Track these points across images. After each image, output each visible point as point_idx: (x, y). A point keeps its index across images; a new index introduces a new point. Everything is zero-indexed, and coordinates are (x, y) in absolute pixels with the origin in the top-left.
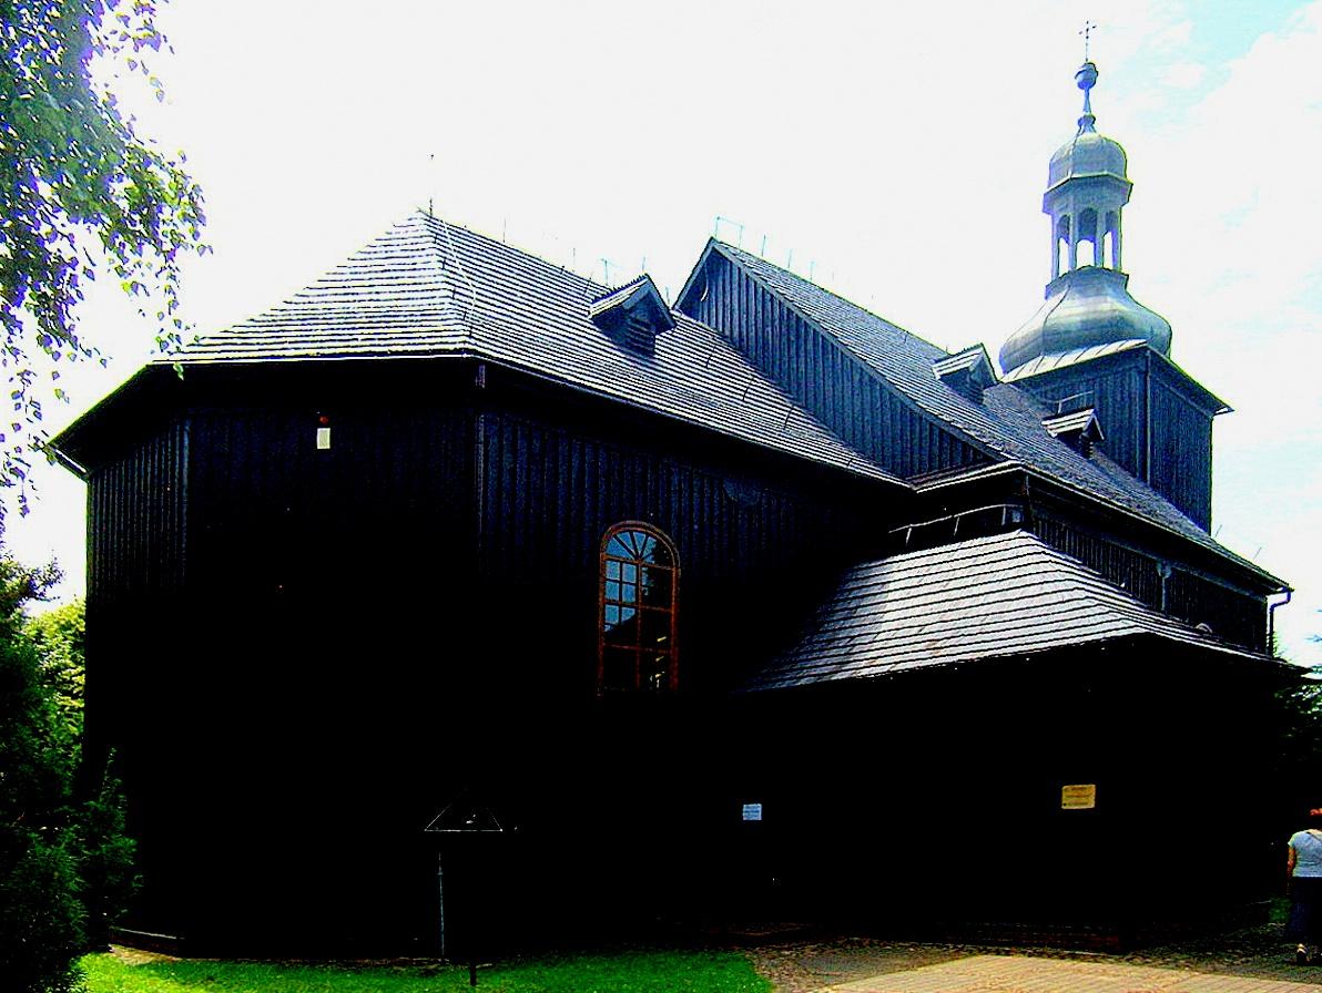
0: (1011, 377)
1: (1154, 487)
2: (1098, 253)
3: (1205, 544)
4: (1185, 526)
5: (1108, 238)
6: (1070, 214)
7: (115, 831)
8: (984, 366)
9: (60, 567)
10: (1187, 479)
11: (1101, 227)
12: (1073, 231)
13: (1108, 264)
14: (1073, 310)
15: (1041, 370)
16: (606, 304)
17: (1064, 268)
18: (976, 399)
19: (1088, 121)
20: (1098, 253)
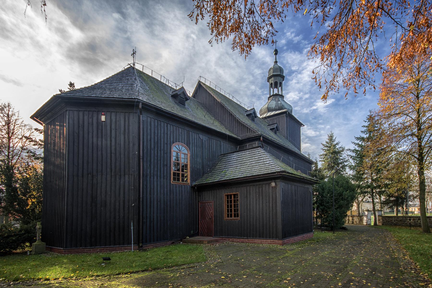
0: (261, 117)
1: (295, 169)
2: (278, 91)
3: (299, 153)
4: (296, 150)
5: (280, 88)
6: (273, 82)
7: (21, 180)
8: (255, 113)
9: (72, 83)
10: (295, 137)
11: (278, 85)
12: (273, 86)
13: (280, 93)
14: (273, 104)
15: (267, 115)
16: (174, 93)
17: (272, 94)
18: (253, 120)
19: (276, 62)
20: (278, 91)
